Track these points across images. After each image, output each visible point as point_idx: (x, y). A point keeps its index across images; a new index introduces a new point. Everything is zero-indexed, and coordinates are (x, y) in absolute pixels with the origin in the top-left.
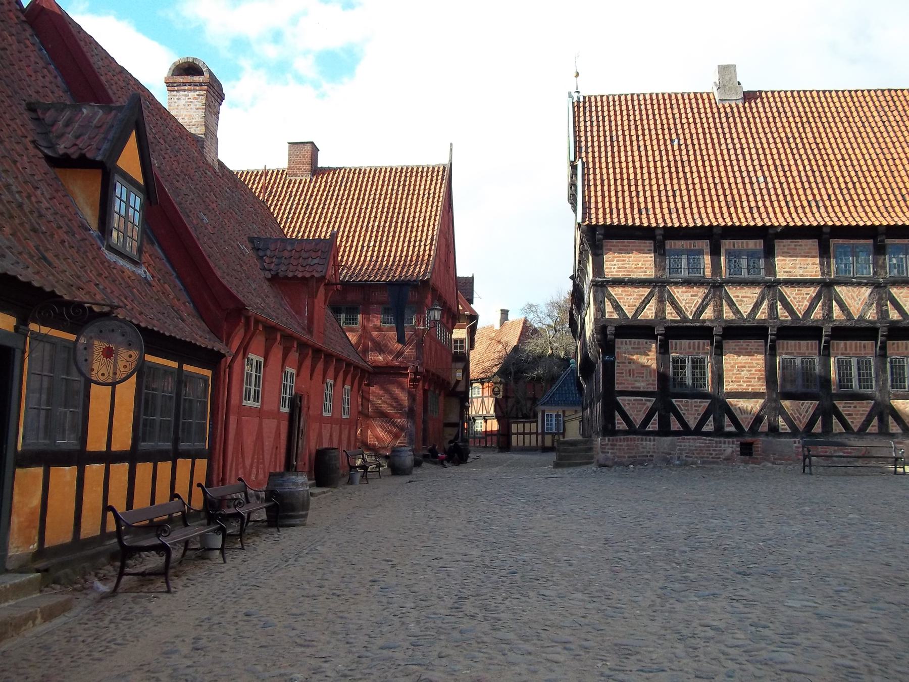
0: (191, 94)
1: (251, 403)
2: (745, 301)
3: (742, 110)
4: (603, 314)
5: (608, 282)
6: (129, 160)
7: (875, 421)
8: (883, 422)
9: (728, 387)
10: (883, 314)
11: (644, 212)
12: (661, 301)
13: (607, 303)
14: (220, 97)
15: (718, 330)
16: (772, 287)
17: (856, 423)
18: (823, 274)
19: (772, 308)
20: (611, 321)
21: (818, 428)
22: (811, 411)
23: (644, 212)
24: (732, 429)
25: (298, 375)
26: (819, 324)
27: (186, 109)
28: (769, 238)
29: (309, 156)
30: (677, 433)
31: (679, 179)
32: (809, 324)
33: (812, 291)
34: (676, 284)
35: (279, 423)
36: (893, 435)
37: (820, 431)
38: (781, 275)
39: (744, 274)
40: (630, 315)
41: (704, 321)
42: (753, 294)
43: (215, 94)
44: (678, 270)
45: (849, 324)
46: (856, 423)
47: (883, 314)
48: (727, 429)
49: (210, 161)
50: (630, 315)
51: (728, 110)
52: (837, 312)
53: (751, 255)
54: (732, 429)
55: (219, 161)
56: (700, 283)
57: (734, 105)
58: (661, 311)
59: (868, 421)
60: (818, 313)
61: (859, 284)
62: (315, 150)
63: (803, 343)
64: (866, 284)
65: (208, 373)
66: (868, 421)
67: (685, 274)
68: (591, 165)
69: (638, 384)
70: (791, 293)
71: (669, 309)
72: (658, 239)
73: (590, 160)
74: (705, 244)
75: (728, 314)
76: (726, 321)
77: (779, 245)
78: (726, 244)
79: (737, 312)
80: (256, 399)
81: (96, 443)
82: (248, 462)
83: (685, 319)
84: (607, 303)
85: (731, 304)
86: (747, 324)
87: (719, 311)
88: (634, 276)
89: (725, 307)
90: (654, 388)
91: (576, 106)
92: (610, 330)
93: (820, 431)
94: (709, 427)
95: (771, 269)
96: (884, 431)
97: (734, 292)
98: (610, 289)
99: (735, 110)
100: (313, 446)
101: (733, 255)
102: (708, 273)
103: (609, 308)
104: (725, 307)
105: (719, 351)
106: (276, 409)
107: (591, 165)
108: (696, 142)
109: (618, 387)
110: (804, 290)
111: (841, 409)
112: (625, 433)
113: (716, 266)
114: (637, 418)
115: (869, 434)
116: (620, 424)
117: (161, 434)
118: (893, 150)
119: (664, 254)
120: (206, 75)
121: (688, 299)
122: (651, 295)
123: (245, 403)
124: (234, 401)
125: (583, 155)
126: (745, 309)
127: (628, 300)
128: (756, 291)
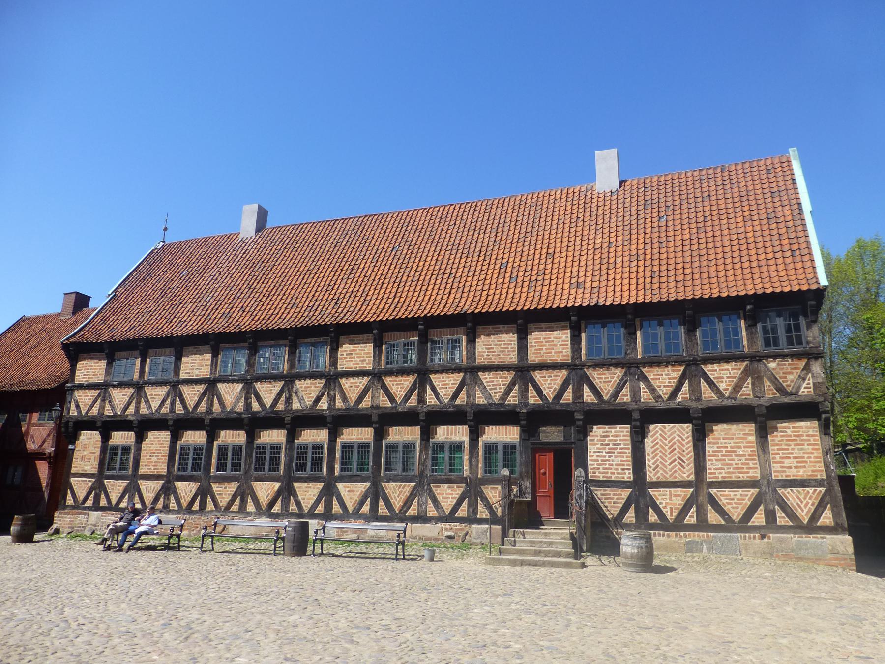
7: (238, 502)
8: (167, 498)
9: (143, 470)
10: (248, 405)
12: (104, 401)
16: (175, 386)
17: (223, 501)
18: (211, 373)
19: (173, 403)
21: (196, 507)
26: (369, 412)
30: (784, 529)
32: (196, 416)
33: (201, 388)
34: (114, 386)
36: (249, 514)
37: (693, 521)
40: (83, 413)
45: (223, 416)
46: (223, 501)
47: (248, 405)
52: (216, 407)
59: (156, 500)
60: (413, 401)
61: (233, 381)
63: (197, 433)
64: (238, 381)
66: (361, 503)
69: (86, 468)
71: (107, 407)
76: (142, 415)
79: (717, 390)
83: (658, 398)
85: (711, 383)
86: (155, 417)
87: (578, 393)
90: (95, 471)
93: (693, 521)
94: (691, 518)
96: (242, 509)
98: (480, 374)
102: (136, 376)
103: (107, 407)
111: (215, 489)
112: (73, 507)
114: (81, 494)
115: (232, 512)
116: (336, 508)
122: (99, 395)
126: (191, 402)
128: (619, 372)
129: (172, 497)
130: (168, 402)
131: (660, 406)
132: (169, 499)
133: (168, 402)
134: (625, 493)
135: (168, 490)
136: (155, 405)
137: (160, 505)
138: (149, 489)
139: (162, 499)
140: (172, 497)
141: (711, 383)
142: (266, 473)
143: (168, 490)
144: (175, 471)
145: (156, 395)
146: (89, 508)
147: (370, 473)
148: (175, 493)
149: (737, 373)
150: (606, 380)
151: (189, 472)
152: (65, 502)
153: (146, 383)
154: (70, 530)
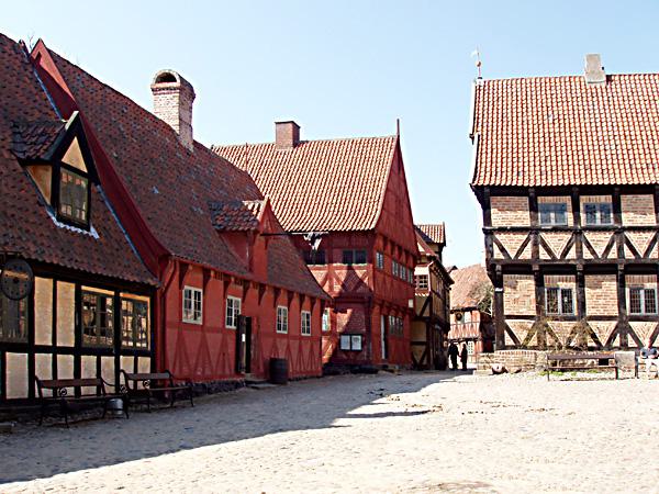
0: (171, 96)
1: (306, 334)
2: (599, 242)
3: (604, 90)
4: (492, 256)
5: (495, 230)
6: (74, 155)
8: (624, 337)
9: (589, 312)
11: (521, 174)
12: (535, 245)
13: (495, 246)
14: (193, 96)
15: (580, 268)
19: (620, 249)
20: (498, 261)
22: (652, 331)
23: (521, 174)
24: (594, 345)
25: (243, 301)
27: (165, 109)
28: (617, 191)
29: (291, 132)
31: (550, 147)
32: (649, 262)
34: (546, 231)
35: (464, 365)
38: (626, 223)
39: (598, 223)
40: (513, 256)
41: (569, 260)
42: (606, 237)
43: (187, 93)
44: (548, 220)
48: (589, 345)
49: (184, 144)
50: (513, 256)
51: (594, 91)
53: (603, 208)
54: (594, 345)
55: (195, 143)
56: (565, 230)
57: (598, 87)
58: (536, 252)
59: (612, 337)
62: (296, 128)
65: (147, 299)
67: (553, 223)
68: (485, 137)
70: (548, 238)
72: (533, 195)
73: (485, 133)
74: (567, 200)
75: (587, 255)
77: (625, 199)
78: (584, 199)
79: (593, 253)
80: (308, 332)
81: (42, 337)
82: (193, 361)
83: (554, 258)
84: (495, 246)
85: (589, 247)
87: (580, 252)
88: (514, 225)
89: (585, 249)
91: (478, 89)
92: (499, 267)
95: (618, 220)
97: (548, 238)
99: (599, 90)
100: (267, 355)
101: (590, 210)
104: (585, 249)
105: (581, 283)
106: (221, 326)
107: (485, 137)
108: (515, 123)
109: (506, 313)
110: (643, 235)
113: (577, 219)
114: (522, 336)
117: (94, 335)
118: (632, 128)
119: (536, 211)
120: (178, 81)
121: (557, 242)
122: (528, 240)
123: (228, 327)
124: (171, 316)
125: (480, 129)
127: (512, 243)
129: (629, 336)
130: (615, 247)
131: (597, 261)
132: (626, 338)
133: (615, 247)
134: (614, 323)
135: (623, 329)
136: (600, 251)
137: (617, 343)
138: (604, 329)
139: (618, 338)
140: (629, 336)
141: (589, 247)
142: (643, 313)
143: (623, 329)
144: (628, 313)
145: (599, 242)
146: (534, 348)
147: (575, 313)
148: (631, 331)
149: (570, 236)
150: (557, 242)
151: (643, 313)
152: (504, 342)
153: (586, 229)
154: (517, 369)
